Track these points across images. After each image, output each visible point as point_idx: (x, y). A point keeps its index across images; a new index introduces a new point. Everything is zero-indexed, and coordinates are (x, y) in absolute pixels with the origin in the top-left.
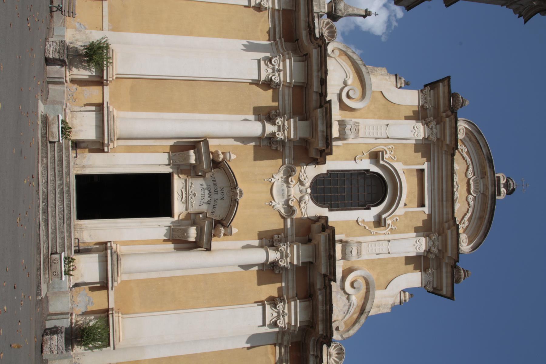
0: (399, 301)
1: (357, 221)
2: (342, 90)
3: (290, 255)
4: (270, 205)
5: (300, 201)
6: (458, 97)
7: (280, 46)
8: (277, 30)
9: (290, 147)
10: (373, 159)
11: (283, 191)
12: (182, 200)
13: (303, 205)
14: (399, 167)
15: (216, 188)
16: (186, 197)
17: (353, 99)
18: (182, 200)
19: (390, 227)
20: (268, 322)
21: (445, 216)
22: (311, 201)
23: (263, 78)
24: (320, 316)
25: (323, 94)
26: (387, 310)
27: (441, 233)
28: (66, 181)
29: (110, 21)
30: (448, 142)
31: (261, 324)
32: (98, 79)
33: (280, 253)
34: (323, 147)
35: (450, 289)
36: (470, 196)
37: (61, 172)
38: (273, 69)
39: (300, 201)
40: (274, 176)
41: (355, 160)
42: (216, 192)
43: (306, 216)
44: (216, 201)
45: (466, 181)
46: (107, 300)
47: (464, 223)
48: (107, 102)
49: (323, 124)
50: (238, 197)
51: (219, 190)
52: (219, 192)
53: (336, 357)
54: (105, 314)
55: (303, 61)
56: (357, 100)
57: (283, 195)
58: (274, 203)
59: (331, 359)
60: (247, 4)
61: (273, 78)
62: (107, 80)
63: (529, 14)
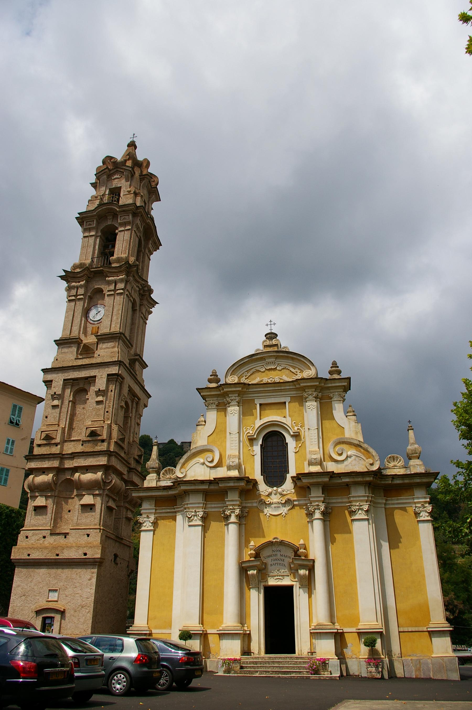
0: (354, 416)
1: (295, 453)
2: (207, 466)
3: (317, 503)
4: (285, 517)
5: (283, 495)
6: (211, 379)
7: (179, 509)
8: (169, 511)
9: (246, 503)
10: (253, 443)
11: (275, 507)
12: (281, 579)
13: (285, 493)
14: (259, 423)
15: (273, 555)
16: (279, 576)
17: (213, 457)
18: (281, 579)
19: (300, 428)
20: (366, 517)
21: (291, 387)
22: (282, 487)
23: (200, 523)
24: (360, 479)
25: (210, 482)
26: (359, 426)
27: (303, 389)
28: (268, 659)
29: (165, 628)
30: (240, 389)
31: (367, 522)
32: (203, 637)
33: (315, 510)
34: (244, 482)
35: (343, 380)
36: (278, 368)
37: (261, 663)
38: (194, 516)
39: (283, 495)
40: (265, 514)
41: (254, 456)
42: (276, 555)
43: (293, 491)
44: (281, 555)
45: (267, 371)
46: (350, 633)
47: (297, 372)
48: (217, 631)
49: (229, 483)
50: (278, 540)
51: (274, 553)
52: (275, 553)
53: (397, 461)
54: (360, 634)
55: (189, 494)
56: (214, 455)
57: (278, 507)
58: (284, 514)
59: (398, 465)
60: (152, 533)
61: (200, 516)
62: (203, 631)
63: (152, 302)
